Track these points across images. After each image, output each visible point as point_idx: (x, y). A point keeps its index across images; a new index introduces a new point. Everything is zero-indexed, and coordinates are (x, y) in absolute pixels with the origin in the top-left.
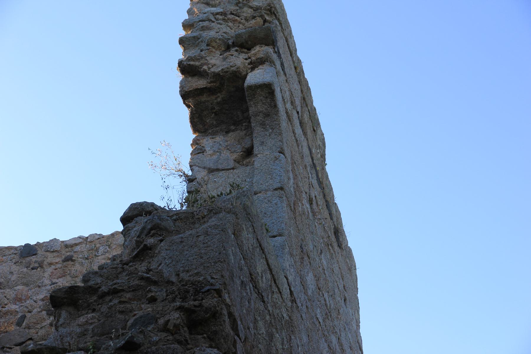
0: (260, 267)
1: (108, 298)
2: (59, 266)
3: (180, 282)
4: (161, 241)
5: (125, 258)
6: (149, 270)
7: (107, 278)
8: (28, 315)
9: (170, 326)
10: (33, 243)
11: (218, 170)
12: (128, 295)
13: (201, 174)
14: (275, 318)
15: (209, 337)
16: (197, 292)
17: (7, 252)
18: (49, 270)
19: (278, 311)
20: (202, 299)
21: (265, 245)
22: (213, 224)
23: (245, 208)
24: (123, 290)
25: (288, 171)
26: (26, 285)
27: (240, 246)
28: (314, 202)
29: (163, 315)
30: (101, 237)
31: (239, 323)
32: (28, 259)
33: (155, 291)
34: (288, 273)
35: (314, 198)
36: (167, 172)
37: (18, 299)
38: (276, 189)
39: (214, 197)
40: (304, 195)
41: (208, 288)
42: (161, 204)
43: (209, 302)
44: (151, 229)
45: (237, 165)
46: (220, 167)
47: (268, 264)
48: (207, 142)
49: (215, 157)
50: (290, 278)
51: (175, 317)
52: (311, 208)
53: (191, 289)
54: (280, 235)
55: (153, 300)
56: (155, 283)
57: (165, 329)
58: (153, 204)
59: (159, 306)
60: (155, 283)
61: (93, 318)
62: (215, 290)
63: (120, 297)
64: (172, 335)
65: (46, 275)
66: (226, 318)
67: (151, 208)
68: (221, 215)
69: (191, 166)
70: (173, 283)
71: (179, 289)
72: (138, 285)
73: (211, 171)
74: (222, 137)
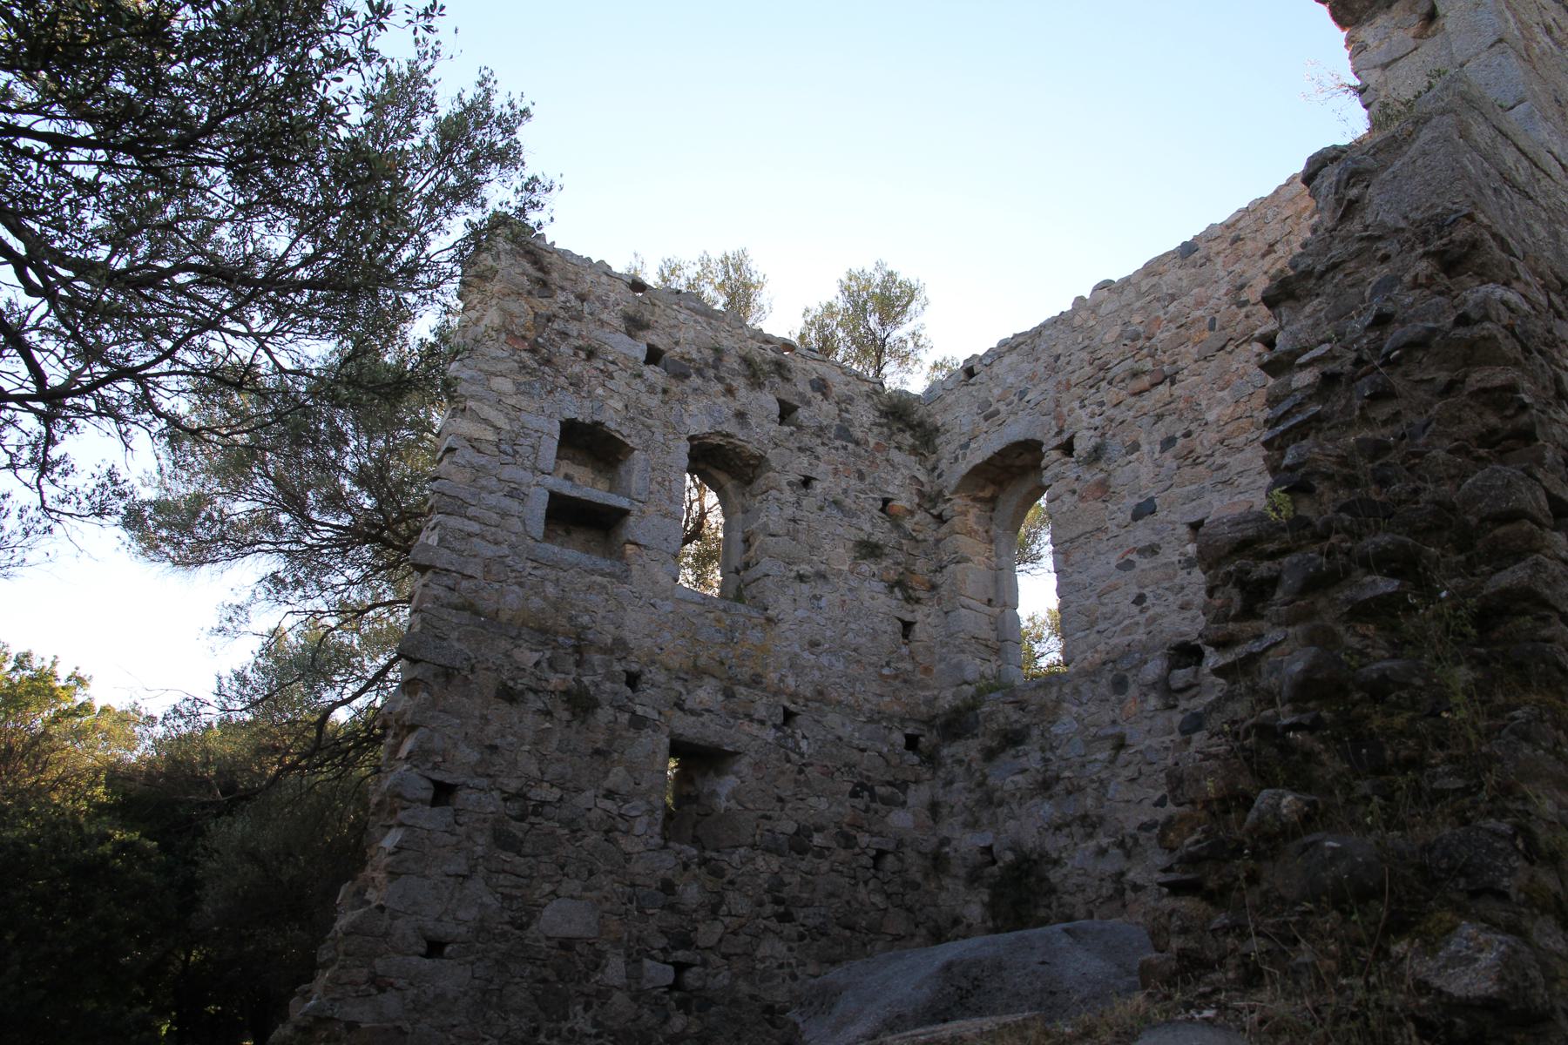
0: (1509, 157)
1: (1328, 277)
2: (1228, 251)
3: (1412, 224)
4: (1367, 187)
5: (1330, 225)
6: (1366, 228)
7: (1318, 255)
8: (1217, 316)
9: (1422, 280)
10: (1188, 239)
11: (1395, 60)
12: (1352, 264)
13: (1374, 77)
14: (1553, 211)
15: (1476, 273)
16: (1439, 228)
17: (1166, 260)
18: (1219, 261)
19: (1553, 200)
20: (1451, 233)
21: (1505, 127)
22: (1429, 137)
23: (1463, 97)
24: (1344, 261)
25: (1501, 12)
26: (1202, 285)
27: (1476, 148)
28: (1555, 29)
29: (1406, 271)
30: (1263, 200)
31: (1509, 240)
32: (1191, 258)
33: (1383, 247)
34: (1550, 145)
35: (1553, 24)
36: (1326, 95)
37: (1199, 304)
38: (1492, 46)
39: (1409, 101)
40: (1536, 29)
41: (1453, 217)
42: (1343, 141)
43: (1460, 234)
44: (1349, 179)
45: (1419, 41)
46: (1397, 55)
47: (1519, 149)
48: (1366, 33)
49: (1384, 47)
50: (1556, 150)
51: (1423, 267)
52: (1553, 39)
53: (1431, 227)
54: (1521, 102)
55: (1385, 258)
56: (1380, 238)
57: (1416, 284)
58: (1335, 147)
59: (1396, 262)
60: (1380, 238)
61: (1320, 303)
62: (1464, 216)
63: (1344, 270)
64: (1428, 288)
65: (1219, 266)
66: (1493, 243)
67: (1334, 153)
68: (1434, 122)
69: (1355, 74)
70: (1403, 230)
71: (1414, 234)
72: (1360, 249)
73: (1385, 66)
74: (1384, 16)
